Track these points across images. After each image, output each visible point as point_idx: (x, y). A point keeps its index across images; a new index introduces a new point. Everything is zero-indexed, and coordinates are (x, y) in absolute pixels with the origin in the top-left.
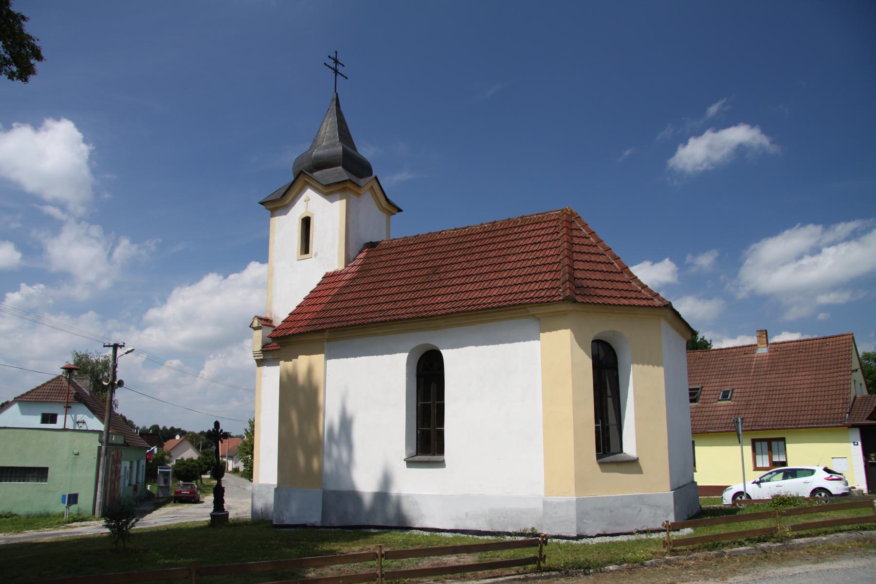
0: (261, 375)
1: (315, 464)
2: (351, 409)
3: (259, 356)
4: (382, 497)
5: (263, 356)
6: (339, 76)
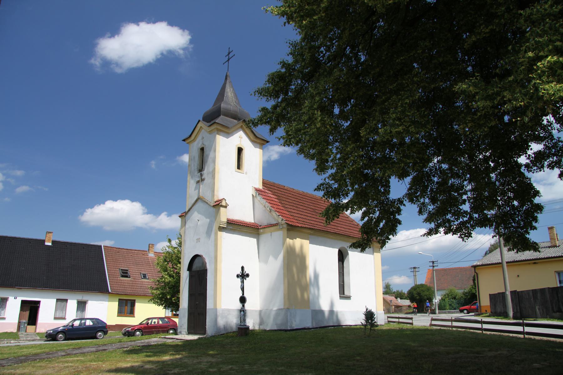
0: (221, 237)
1: (306, 295)
2: (318, 269)
4: (332, 312)
5: (226, 226)
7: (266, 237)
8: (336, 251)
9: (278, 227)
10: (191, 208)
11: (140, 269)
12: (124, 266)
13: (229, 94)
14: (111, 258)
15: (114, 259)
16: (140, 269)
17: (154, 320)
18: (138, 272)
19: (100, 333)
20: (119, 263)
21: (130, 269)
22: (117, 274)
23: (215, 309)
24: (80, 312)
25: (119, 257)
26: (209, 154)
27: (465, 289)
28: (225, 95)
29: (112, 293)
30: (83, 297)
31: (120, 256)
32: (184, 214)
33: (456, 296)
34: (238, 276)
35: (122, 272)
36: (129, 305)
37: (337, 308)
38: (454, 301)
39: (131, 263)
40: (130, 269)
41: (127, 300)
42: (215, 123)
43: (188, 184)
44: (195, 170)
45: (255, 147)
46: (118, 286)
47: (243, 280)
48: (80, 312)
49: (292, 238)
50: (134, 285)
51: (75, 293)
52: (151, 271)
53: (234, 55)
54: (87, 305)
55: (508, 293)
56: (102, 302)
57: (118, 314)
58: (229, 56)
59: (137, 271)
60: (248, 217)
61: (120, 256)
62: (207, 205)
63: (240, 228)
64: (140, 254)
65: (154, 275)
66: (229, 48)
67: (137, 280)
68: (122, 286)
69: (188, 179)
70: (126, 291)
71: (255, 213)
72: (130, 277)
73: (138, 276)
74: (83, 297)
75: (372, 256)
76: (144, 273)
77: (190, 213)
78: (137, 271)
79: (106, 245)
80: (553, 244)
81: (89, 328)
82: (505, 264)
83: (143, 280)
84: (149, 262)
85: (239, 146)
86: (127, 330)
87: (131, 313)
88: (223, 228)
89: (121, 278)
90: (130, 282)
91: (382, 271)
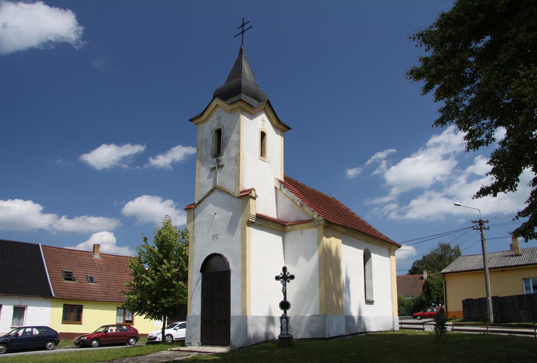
0: (249, 233)
3: (253, 219)
4: (360, 317)
5: (256, 220)
7: (293, 235)
8: (362, 252)
10: (203, 199)
11: (85, 272)
12: (67, 268)
13: (246, 70)
14: (52, 259)
15: (55, 260)
16: (85, 272)
17: (110, 328)
18: (84, 274)
19: (49, 344)
20: (60, 265)
21: (74, 271)
22: (60, 277)
23: (244, 318)
24: (16, 319)
25: (60, 258)
26: (230, 137)
27: (414, 297)
28: (243, 72)
29: (56, 298)
30: (21, 302)
31: (62, 256)
32: (193, 206)
33: (404, 303)
34: (277, 278)
35: (66, 274)
36: (75, 311)
37: (364, 314)
38: (402, 308)
39: (75, 264)
40: (74, 271)
41: (73, 306)
42: (241, 100)
43: (197, 171)
44: (207, 155)
46: (62, 290)
47: (286, 283)
48: (16, 319)
49: (327, 237)
50: (80, 288)
51: (11, 298)
52: (98, 273)
53: (251, 27)
54: (25, 311)
55: (490, 299)
56: (43, 308)
57: (62, 321)
58: (243, 28)
59: (82, 274)
60: (272, 214)
61: (62, 256)
62: (229, 196)
63: (268, 223)
64: (84, 255)
65: (102, 278)
66: (243, 19)
67: (83, 284)
68: (67, 290)
69: (197, 165)
70: (72, 296)
71: (278, 208)
72: (75, 281)
73: (84, 279)
74: (21, 302)
75: (387, 259)
76: (90, 276)
77: (201, 205)
78: (82, 274)
79: (43, 244)
80: (517, 252)
81: (36, 338)
82: (487, 270)
83: (90, 284)
84: (95, 264)
85: (262, 131)
86: (82, 339)
87: (78, 320)
88: (252, 222)
89: (65, 281)
90: (76, 286)
91: (397, 276)
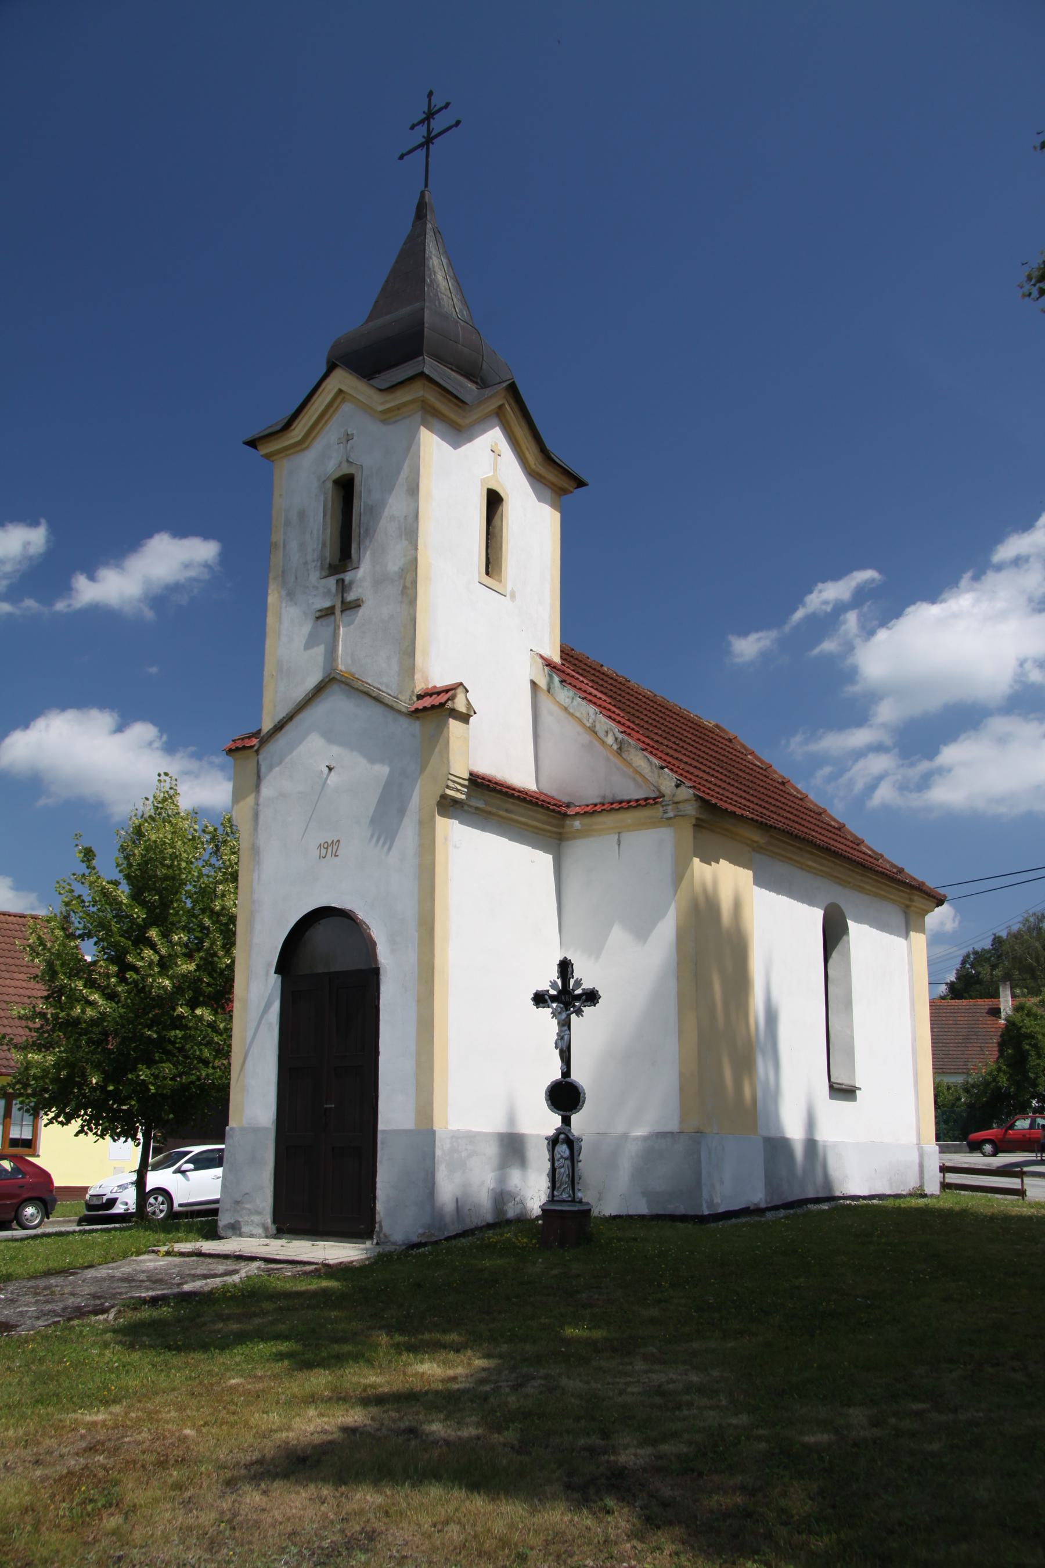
3: (458, 790)
4: (811, 1144)
5: (468, 795)
6: (421, 153)
9: (657, 812)
10: (290, 718)
13: (440, 277)
26: (383, 503)
32: (255, 742)
45: (540, 499)
49: (706, 860)
62: (377, 709)
66: (430, 94)
69: (272, 598)
71: (541, 755)
75: (899, 942)
85: (490, 487)
88: (455, 802)
